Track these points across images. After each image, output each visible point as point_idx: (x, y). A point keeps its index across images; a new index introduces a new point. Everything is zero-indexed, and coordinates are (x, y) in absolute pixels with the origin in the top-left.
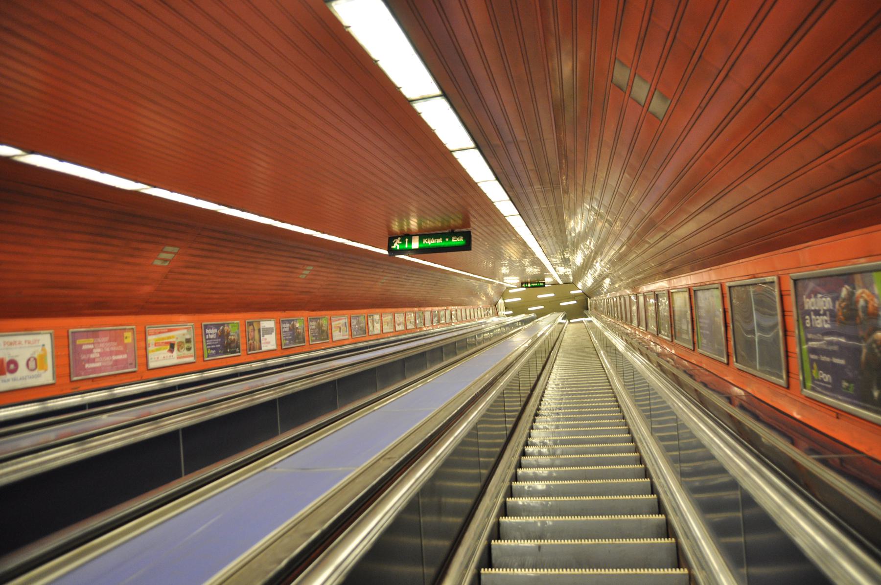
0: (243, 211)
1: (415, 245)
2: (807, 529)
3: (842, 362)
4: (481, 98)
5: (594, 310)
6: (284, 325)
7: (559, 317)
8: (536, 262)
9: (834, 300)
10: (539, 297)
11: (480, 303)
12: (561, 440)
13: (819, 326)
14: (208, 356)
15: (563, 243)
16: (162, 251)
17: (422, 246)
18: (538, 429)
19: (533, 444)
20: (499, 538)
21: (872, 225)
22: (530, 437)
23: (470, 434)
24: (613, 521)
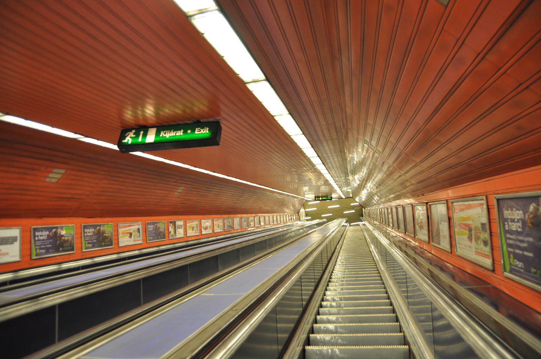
1: (151, 138)
3: (531, 255)
4: (311, 122)
5: (367, 217)
6: (149, 227)
7: (343, 221)
8: (326, 183)
9: (524, 214)
10: (329, 207)
11: (287, 210)
13: (514, 229)
14: (86, 249)
15: (345, 171)
16: (51, 172)
17: (158, 139)
18: (330, 290)
19: (327, 300)
20: (313, 333)
21: (511, 172)
22: (325, 295)
23: (287, 293)
24: (376, 349)
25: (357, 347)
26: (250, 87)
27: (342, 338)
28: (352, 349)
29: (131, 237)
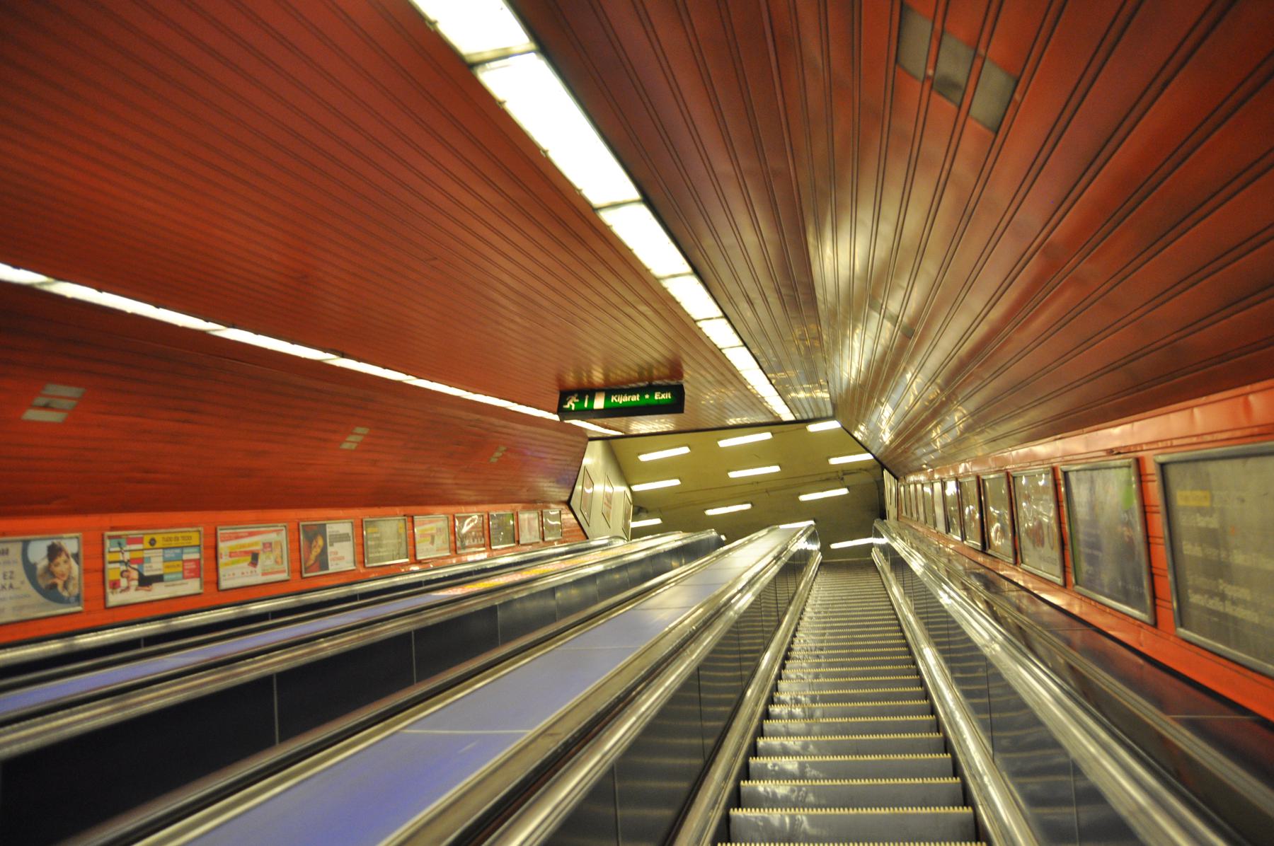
0: (385, 367)
1: (599, 403)
2: (1122, 780)
12: (821, 696)
15: (796, 310)
17: (609, 406)
18: (788, 678)
20: (748, 778)
25: (853, 812)
26: (607, 217)
27: (815, 790)
28: (841, 816)
29: (432, 543)
